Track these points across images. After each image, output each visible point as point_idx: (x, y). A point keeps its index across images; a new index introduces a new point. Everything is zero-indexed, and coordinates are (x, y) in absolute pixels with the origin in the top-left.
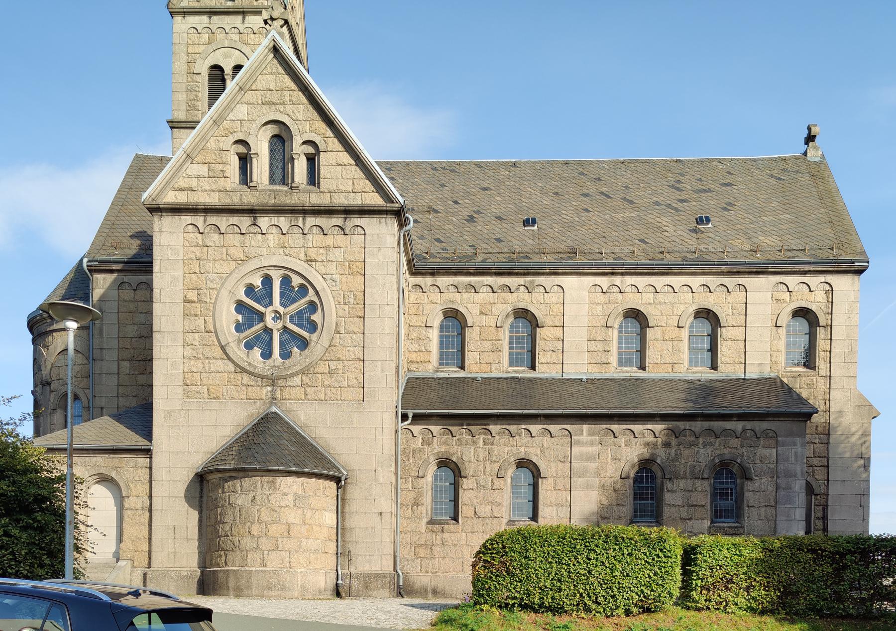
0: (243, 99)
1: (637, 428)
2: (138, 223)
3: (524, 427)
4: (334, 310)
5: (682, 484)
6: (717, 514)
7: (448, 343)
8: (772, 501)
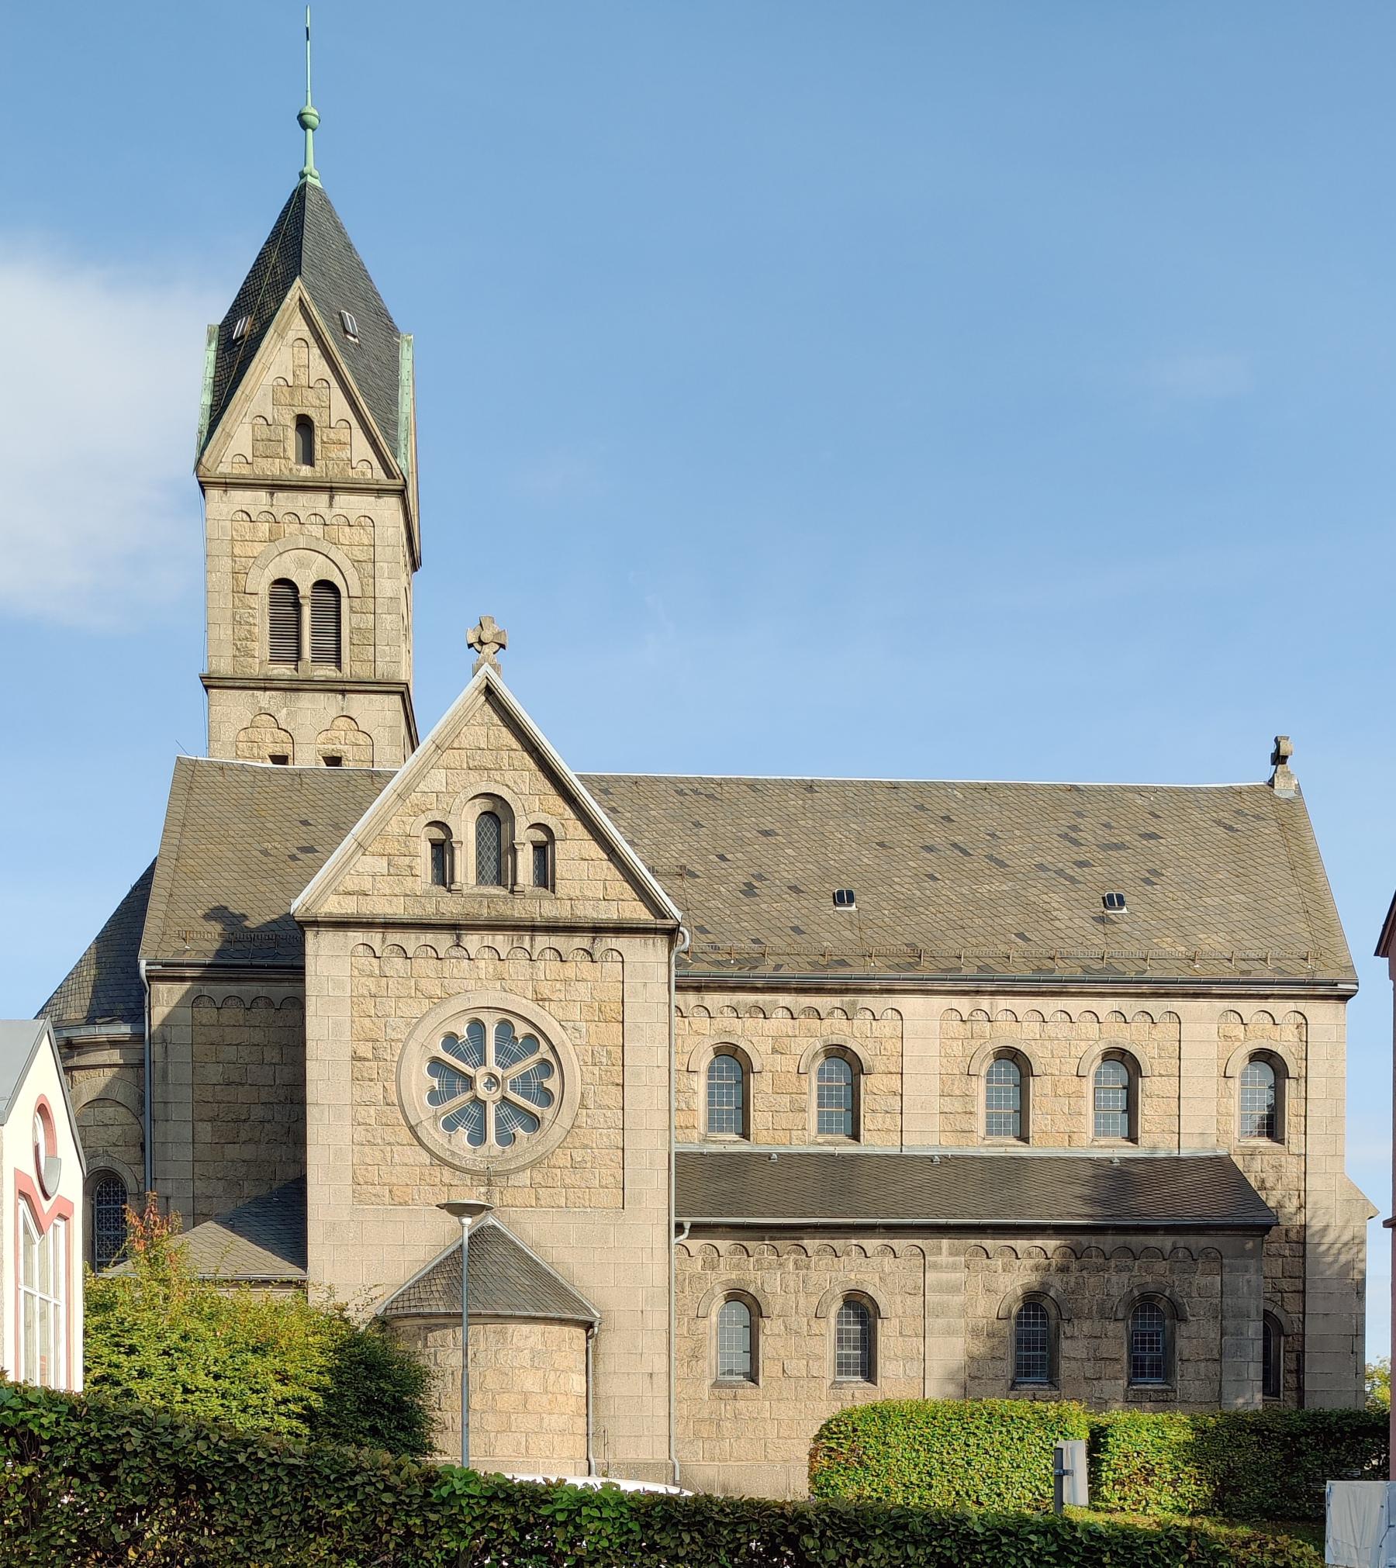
0: (440, 762)
1: (1021, 1244)
2: (210, 891)
3: (854, 1242)
4: (578, 1074)
5: (1086, 1327)
6: (1138, 1369)
7: (721, 1095)
8: (1215, 1352)
